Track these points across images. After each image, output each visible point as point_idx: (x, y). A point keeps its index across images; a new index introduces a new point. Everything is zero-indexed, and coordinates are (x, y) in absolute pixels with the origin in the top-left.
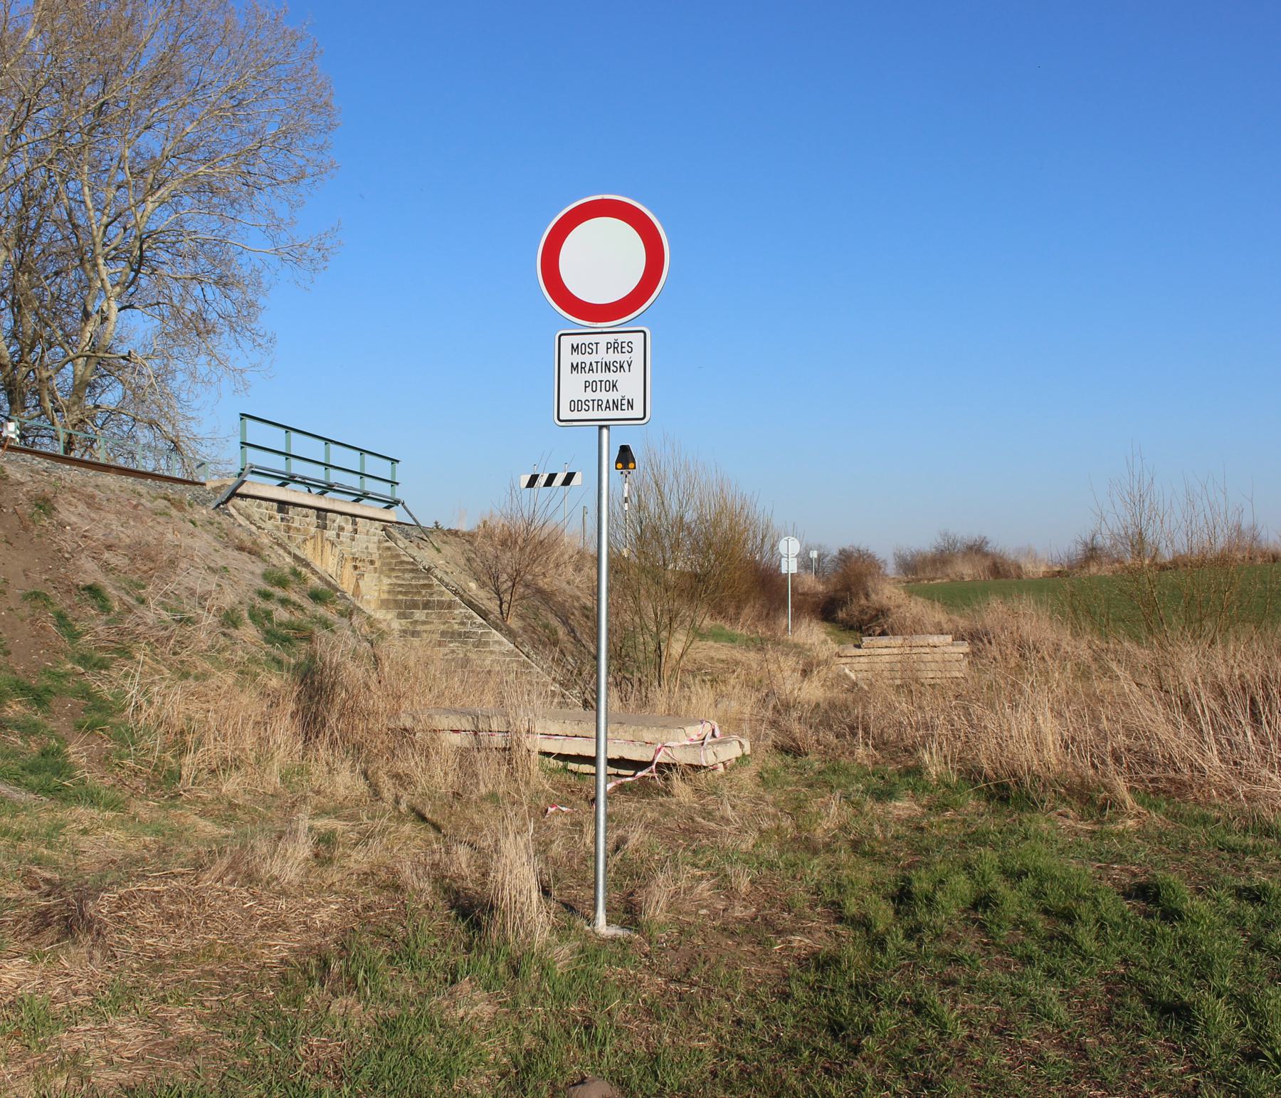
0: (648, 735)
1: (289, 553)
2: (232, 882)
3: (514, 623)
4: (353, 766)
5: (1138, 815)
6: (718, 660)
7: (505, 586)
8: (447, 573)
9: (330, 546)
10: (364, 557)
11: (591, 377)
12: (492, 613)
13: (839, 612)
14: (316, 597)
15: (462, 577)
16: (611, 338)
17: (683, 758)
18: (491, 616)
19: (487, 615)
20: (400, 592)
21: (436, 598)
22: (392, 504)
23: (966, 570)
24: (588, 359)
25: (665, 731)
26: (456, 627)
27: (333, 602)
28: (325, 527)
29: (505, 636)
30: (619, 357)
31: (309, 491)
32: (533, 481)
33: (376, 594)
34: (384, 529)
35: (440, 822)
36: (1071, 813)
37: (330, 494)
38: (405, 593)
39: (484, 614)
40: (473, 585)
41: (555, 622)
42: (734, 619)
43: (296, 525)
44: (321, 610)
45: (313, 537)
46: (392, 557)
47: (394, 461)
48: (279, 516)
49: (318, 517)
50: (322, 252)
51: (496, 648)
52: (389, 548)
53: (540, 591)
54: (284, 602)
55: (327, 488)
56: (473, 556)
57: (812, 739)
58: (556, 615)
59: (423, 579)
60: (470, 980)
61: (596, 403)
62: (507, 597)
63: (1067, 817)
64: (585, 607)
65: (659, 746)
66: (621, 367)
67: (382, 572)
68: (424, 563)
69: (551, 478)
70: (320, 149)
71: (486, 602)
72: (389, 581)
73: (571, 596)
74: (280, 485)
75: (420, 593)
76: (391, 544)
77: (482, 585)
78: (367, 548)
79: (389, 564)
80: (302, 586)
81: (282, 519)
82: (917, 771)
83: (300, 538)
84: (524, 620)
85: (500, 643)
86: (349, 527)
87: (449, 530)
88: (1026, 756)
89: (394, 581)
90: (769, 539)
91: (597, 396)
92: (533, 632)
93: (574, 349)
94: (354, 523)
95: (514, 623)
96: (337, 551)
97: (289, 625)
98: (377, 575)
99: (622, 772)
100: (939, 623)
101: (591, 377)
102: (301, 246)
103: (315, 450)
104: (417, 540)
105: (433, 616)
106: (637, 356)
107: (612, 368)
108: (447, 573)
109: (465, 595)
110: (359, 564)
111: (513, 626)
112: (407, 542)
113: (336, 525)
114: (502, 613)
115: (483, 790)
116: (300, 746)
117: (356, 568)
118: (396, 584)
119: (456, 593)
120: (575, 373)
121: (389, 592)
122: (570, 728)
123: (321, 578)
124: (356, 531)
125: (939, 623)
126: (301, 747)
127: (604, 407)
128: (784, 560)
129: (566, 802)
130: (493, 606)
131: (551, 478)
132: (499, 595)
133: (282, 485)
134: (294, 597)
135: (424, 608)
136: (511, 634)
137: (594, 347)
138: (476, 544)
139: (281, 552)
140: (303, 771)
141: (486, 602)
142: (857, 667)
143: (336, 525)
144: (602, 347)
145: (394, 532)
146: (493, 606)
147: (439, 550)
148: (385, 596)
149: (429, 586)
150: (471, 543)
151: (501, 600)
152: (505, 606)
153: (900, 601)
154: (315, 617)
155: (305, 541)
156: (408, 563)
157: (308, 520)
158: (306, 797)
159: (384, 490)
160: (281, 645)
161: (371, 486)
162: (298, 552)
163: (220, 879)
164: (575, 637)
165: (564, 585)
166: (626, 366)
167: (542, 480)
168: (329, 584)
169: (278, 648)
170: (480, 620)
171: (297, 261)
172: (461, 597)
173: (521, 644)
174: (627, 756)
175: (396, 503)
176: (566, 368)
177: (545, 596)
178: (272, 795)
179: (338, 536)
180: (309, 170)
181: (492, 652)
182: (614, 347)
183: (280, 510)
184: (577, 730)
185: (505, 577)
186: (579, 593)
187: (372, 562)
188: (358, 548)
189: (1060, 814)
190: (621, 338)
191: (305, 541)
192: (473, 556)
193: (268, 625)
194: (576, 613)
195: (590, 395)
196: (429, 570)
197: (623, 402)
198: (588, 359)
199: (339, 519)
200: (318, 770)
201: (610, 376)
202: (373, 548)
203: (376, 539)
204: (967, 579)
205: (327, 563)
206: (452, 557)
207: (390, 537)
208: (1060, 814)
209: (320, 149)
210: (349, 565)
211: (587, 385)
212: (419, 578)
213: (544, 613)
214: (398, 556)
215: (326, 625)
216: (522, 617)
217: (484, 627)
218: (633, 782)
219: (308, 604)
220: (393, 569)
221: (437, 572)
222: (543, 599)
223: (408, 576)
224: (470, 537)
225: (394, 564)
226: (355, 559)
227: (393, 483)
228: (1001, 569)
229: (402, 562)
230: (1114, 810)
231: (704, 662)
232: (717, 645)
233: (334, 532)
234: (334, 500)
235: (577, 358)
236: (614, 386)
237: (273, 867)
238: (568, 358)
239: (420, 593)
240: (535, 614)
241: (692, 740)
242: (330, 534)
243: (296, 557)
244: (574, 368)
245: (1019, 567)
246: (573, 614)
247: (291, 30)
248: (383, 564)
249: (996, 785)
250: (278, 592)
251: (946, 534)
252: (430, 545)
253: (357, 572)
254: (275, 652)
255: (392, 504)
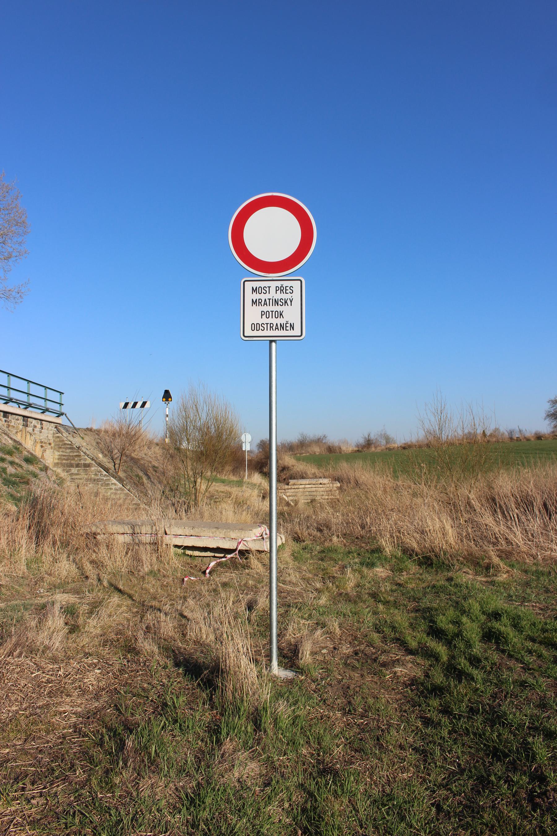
0: (233, 535)
1: (11, 438)
2: (19, 656)
3: (121, 474)
4: (68, 557)
5: (508, 572)
6: (220, 491)
7: (116, 456)
8: (87, 449)
9: (29, 435)
10: (46, 441)
11: (265, 308)
12: (110, 469)
13: (264, 469)
14: (28, 460)
15: (95, 451)
16: (279, 284)
17: (254, 546)
18: (110, 471)
19: (108, 470)
20: (64, 459)
21: (82, 462)
22: (60, 415)
23: (317, 450)
24: (263, 297)
25: (243, 532)
26: (93, 476)
27: (37, 463)
28: (27, 426)
29: (118, 480)
30: (284, 296)
31: (19, 407)
32: (126, 405)
33: (52, 460)
34: (56, 427)
35: (132, 592)
36: (470, 572)
37: (30, 409)
38: (67, 460)
39: (107, 470)
40: (100, 456)
41: (141, 474)
42: (221, 472)
43: (12, 424)
44: (31, 468)
45: (21, 431)
46: (60, 441)
47: (61, 393)
48: (4, 419)
49: (24, 420)
50: (20, 294)
51: (113, 487)
52: (58, 437)
53: (132, 459)
54: (12, 463)
55: (29, 406)
56: (100, 441)
57: (305, 534)
58: (141, 470)
59: (76, 452)
60: (231, 740)
61: (269, 325)
62: (117, 462)
63: (468, 573)
64: (154, 466)
65: (240, 540)
66: (286, 302)
67: (55, 449)
68: (76, 445)
69: (135, 404)
70: (20, 243)
71: (107, 464)
72: (59, 453)
73: (147, 461)
74: (5, 403)
75: (74, 459)
76: (60, 435)
77: (105, 456)
78: (47, 437)
79: (59, 445)
80: (20, 455)
81: (5, 421)
82: (379, 550)
83: (14, 431)
84: (126, 473)
85: (115, 484)
86: (39, 426)
87: (87, 429)
88: (438, 542)
89: (61, 453)
90: (232, 434)
91: (270, 321)
92: (131, 479)
93: (254, 290)
94: (42, 424)
95: (121, 474)
96: (33, 438)
97: (16, 476)
98: (52, 450)
99: (217, 555)
100: (315, 473)
101: (265, 308)
102: (10, 291)
103: (22, 386)
104: (72, 433)
105: (81, 471)
106: (296, 296)
107: (280, 303)
108: (87, 449)
109: (97, 461)
110: (43, 445)
111: (121, 476)
112: (67, 434)
113: (32, 425)
114: (115, 469)
115: (146, 569)
116: (34, 546)
117: (42, 447)
118: (62, 455)
119: (93, 459)
120: (254, 306)
121: (58, 459)
122: (188, 531)
123: (28, 452)
124: (42, 428)
125: (315, 473)
126: (35, 546)
127: (274, 328)
128: (244, 444)
129: (192, 574)
130: (110, 466)
131: (135, 404)
132: (113, 460)
133: (6, 403)
134: (17, 461)
135: (76, 467)
136: (120, 480)
137: (267, 289)
138: (101, 435)
139: (6, 437)
140: (37, 560)
141: (107, 464)
142: (288, 494)
143: (32, 425)
144: (273, 290)
145: (61, 429)
146: (110, 466)
147: (83, 438)
148: (56, 461)
149: (79, 456)
150: (99, 435)
151: (114, 463)
152: (117, 466)
153: (294, 464)
154: (29, 471)
155: (17, 432)
156: (68, 444)
157: (18, 422)
158: (43, 578)
159: (56, 407)
160: (12, 486)
161: (50, 405)
162: (14, 437)
163: (10, 654)
164: (151, 481)
165: (144, 456)
166: (289, 302)
167: (130, 405)
168: (32, 454)
169: (11, 488)
170: (105, 473)
171: (8, 298)
172: (95, 461)
173: (126, 485)
174: (221, 547)
175: (62, 414)
176: (248, 302)
177: (135, 461)
178: (22, 578)
179: (33, 430)
180: (14, 254)
181: (111, 489)
182: (281, 289)
183: (5, 416)
184: (192, 532)
185: (116, 451)
186: (151, 460)
187: (50, 444)
188: (43, 437)
189: (464, 572)
190: (285, 284)
191: (17, 432)
192: (100, 441)
193: (4, 475)
194: (150, 469)
195: (264, 320)
196: (79, 448)
197: (287, 325)
198: (263, 297)
199: (34, 422)
200: (47, 559)
201: (278, 308)
202: (50, 437)
203: (52, 432)
204: (317, 454)
205: (28, 444)
206: (90, 441)
207: (59, 431)
208: (464, 572)
209: (20, 243)
210: (39, 446)
211: (263, 314)
212: (74, 452)
213: (135, 469)
214: (63, 441)
215: (35, 476)
216: (125, 471)
217: (107, 476)
218: (226, 561)
219: (24, 464)
220: (61, 448)
221: (83, 449)
222: (135, 462)
223: (68, 451)
224: (98, 432)
225: (61, 445)
226: (41, 442)
227: (61, 404)
228: (332, 449)
229: (65, 444)
230: (493, 569)
231: (213, 492)
232: (217, 484)
233: (32, 429)
234: (32, 412)
235: (256, 296)
236: (281, 314)
237: (42, 638)
238: (250, 296)
239: (74, 459)
240: (131, 470)
241: (257, 537)
242: (30, 429)
243: (15, 441)
244: (254, 302)
245: (340, 448)
246: (149, 470)
247: (6, 185)
248: (55, 445)
249: (422, 557)
250: (8, 457)
251: (302, 434)
252: (79, 436)
253: (43, 449)
254: (10, 490)
255: (60, 415)
